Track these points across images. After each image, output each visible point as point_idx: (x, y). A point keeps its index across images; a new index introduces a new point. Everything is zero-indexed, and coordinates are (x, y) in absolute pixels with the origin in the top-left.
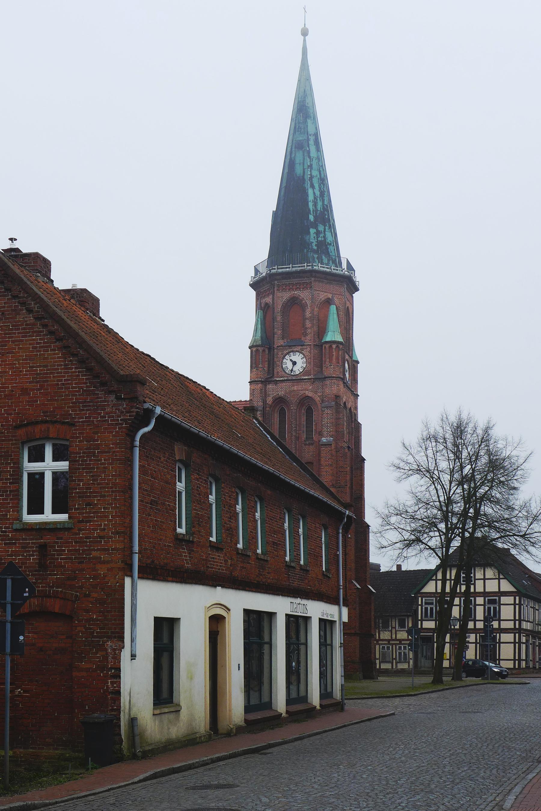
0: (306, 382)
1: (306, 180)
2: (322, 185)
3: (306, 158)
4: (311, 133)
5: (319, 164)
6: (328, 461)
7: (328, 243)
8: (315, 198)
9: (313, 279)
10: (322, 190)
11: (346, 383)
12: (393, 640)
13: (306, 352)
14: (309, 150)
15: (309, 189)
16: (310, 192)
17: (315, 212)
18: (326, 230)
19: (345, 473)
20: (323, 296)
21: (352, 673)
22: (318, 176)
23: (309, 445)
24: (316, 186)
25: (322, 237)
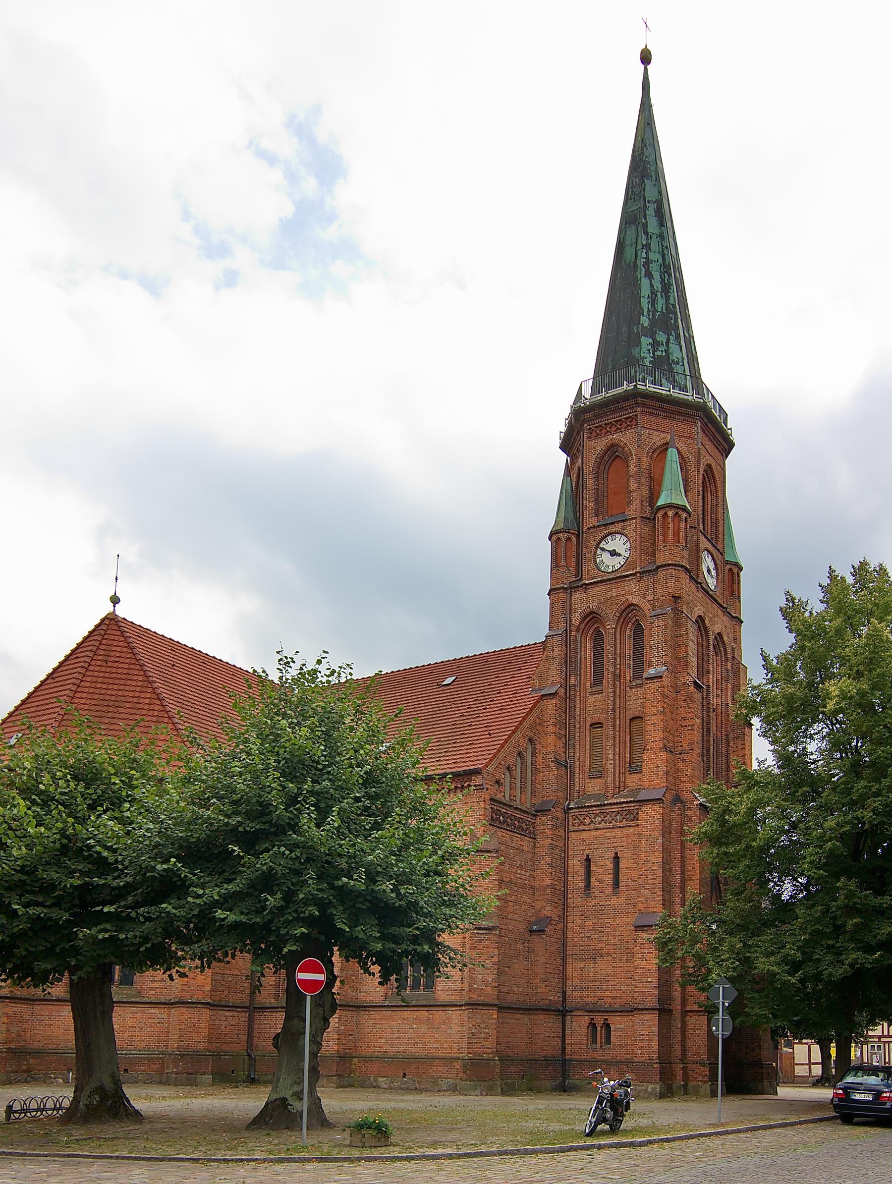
0: (629, 580)
1: (639, 267)
2: (666, 274)
3: (640, 234)
4: (650, 199)
5: (662, 243)
6: (656, 706)
7: (673, 361)
8: (653, 292)
9: (639, 409)
10: (666, 282)
11: (701, 584)
12: (885, 1037)
13: (631, 527)
14: (647, 222)
15: (643, 279)
16: (645, 283)
17: (651, 313)
18: (671, 341)
19: (689, 728)
20: (658, 439)
21: (700, 1083)
22: (660, 261)
23: (637, 686)
24: (656, 275)
25: (662, 351)
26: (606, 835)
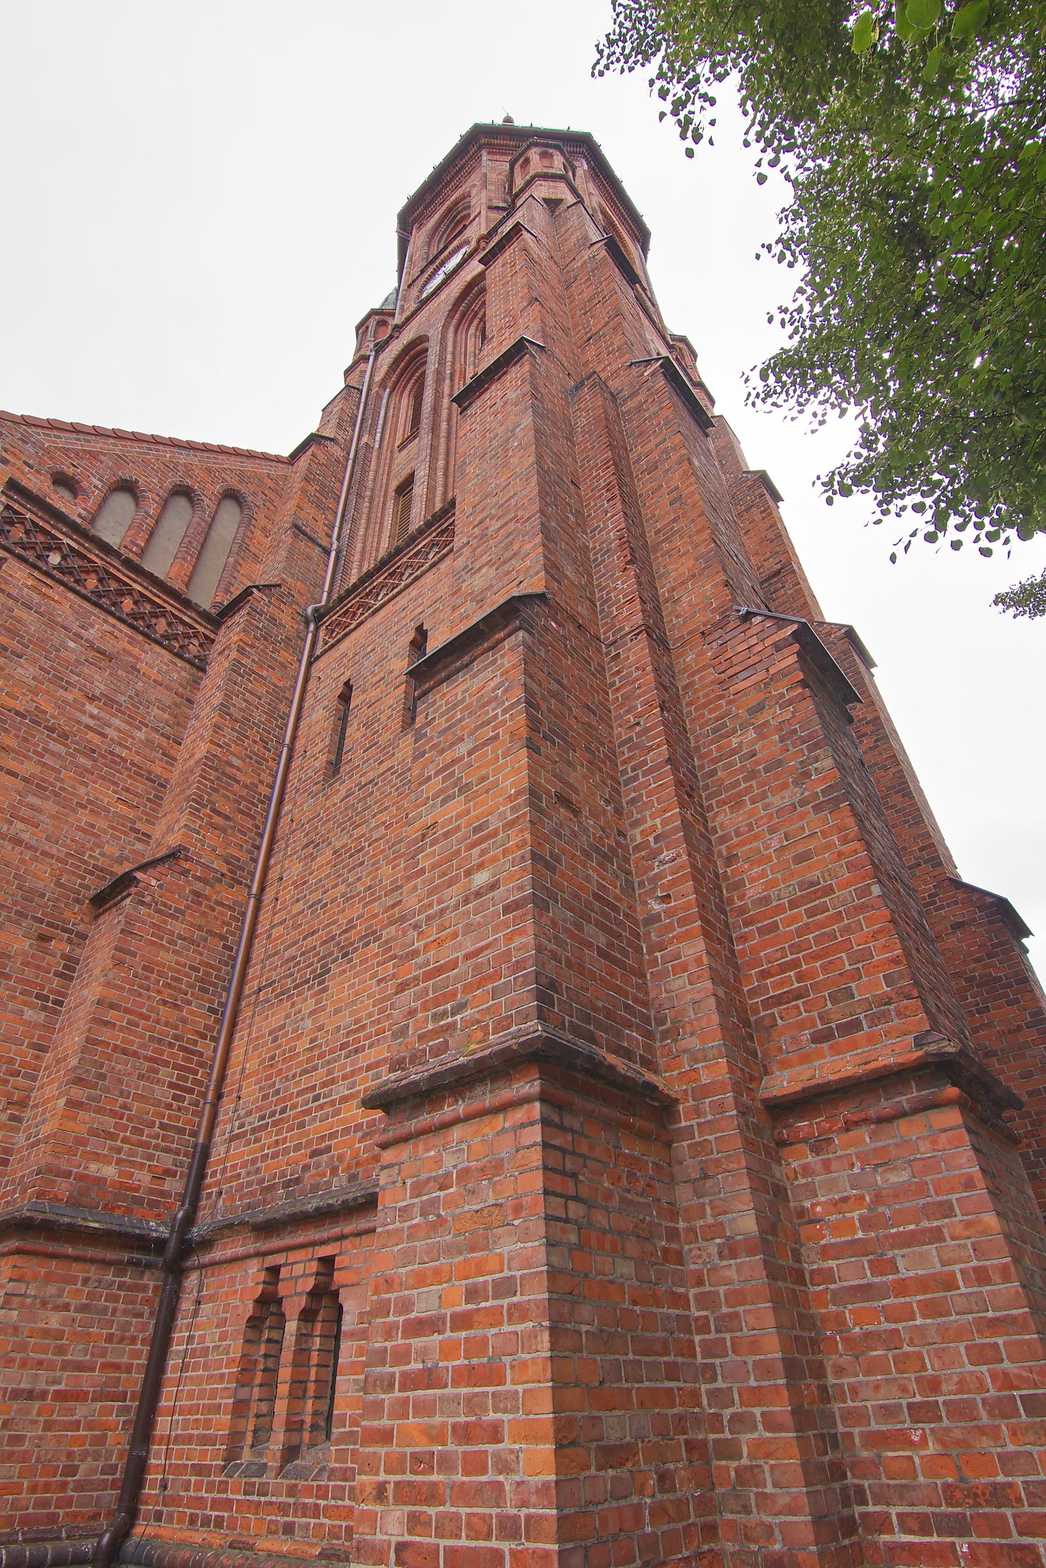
26: (398, 606)
